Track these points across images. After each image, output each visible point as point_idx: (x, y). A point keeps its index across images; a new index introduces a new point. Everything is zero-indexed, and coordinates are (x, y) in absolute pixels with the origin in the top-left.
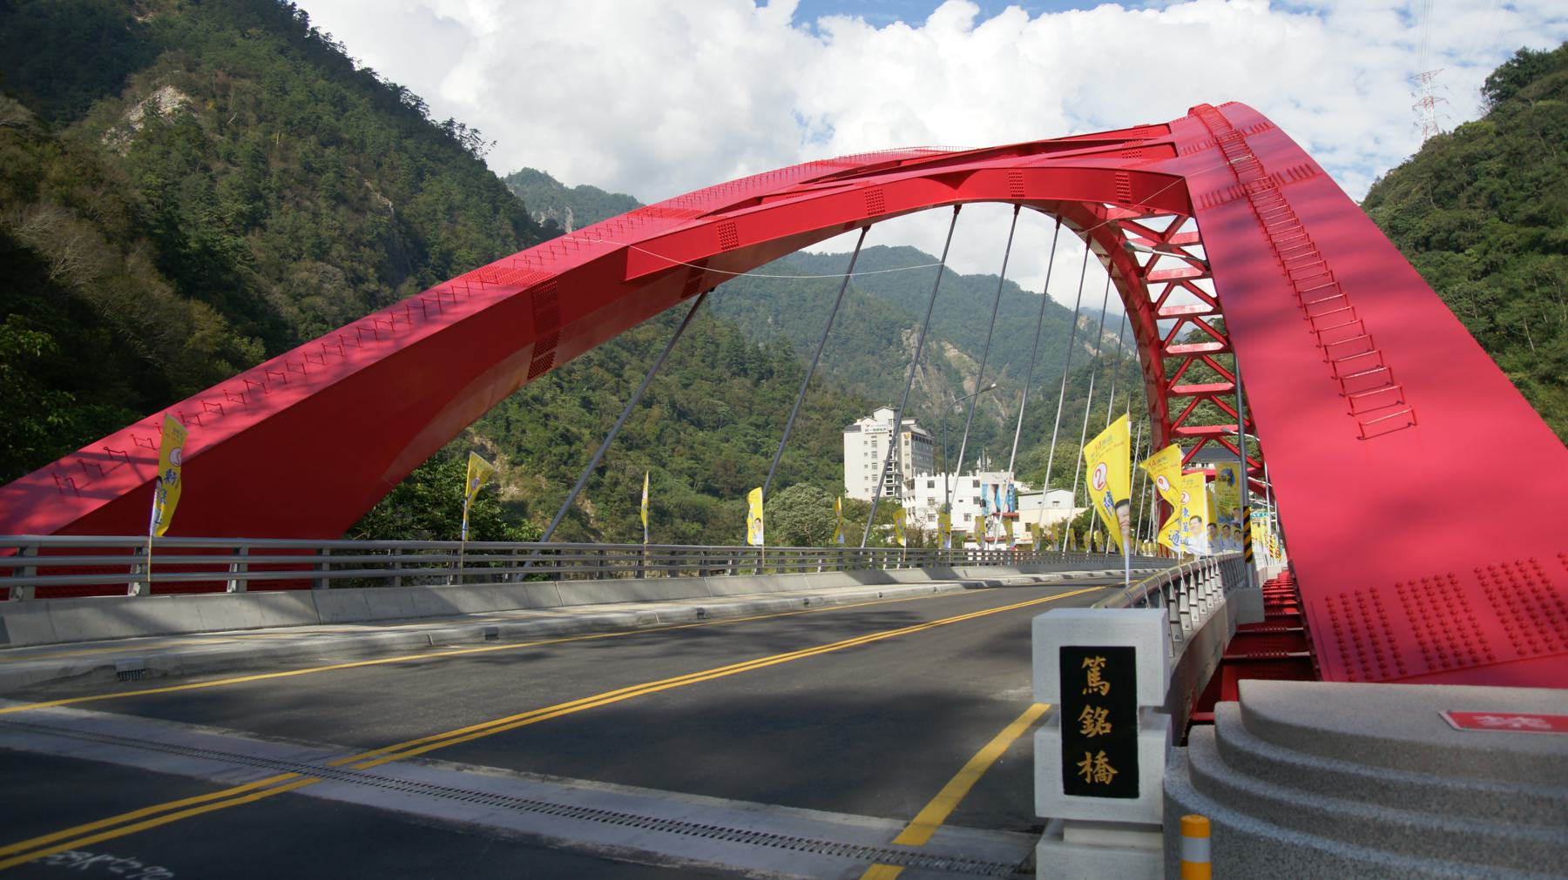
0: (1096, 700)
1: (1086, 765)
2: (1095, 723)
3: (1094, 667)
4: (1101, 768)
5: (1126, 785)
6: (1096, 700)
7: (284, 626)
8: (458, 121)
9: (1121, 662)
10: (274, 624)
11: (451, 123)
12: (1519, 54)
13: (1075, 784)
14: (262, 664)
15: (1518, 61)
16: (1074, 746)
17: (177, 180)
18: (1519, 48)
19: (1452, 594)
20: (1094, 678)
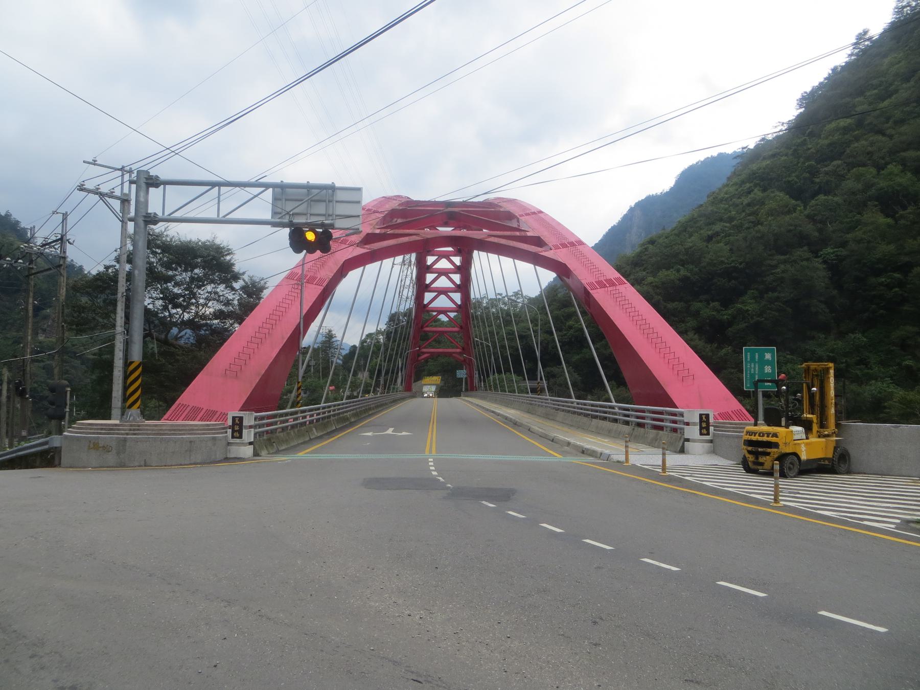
0: (704, 422)
4: (704, 431)
5: (708, 434)
9: (707, 416)
13: (701, 434)
20: (704, 418)
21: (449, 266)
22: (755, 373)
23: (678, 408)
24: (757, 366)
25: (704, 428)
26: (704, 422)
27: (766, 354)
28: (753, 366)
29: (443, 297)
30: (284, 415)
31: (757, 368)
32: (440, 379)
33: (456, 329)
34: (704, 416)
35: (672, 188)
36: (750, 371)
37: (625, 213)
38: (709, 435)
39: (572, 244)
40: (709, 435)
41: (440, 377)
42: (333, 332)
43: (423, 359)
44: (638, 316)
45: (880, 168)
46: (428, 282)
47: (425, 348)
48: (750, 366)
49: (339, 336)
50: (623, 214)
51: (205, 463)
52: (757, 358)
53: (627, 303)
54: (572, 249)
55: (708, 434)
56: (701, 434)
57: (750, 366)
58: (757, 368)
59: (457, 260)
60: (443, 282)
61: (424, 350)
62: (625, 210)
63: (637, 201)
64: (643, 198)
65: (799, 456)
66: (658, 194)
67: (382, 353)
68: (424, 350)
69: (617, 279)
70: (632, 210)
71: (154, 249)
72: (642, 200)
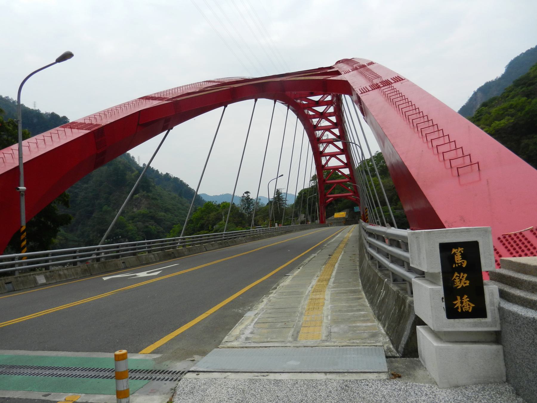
0: (460, 269)
20: (458, 259)
21: (333, 137)
23: (446, 228)
25: (463, 291)
26: (460, 269)
29: (333, 159)
30: (128, 246)
32: (345, 214)
35: (503, 74)
37: (471, 97)
38: (484, 315)
39: (387, 83)
40: (484, 315)
41: (345, 212)
42: (280, 191)
43: (329, 202)
44: (428, 121)
46: (321, 149)
49: (284, 191)
50: (469, 97)
51: (11, 292)
53: (401, 96)
54: (386, 89)
59: (336, 131)
60: (331, 149)
61: (329, 196)
62: (471, 94)
63: (478, 87)
66: (494, 80)
68: (329, 196)
70: (475, 94)
72: (482, 86)
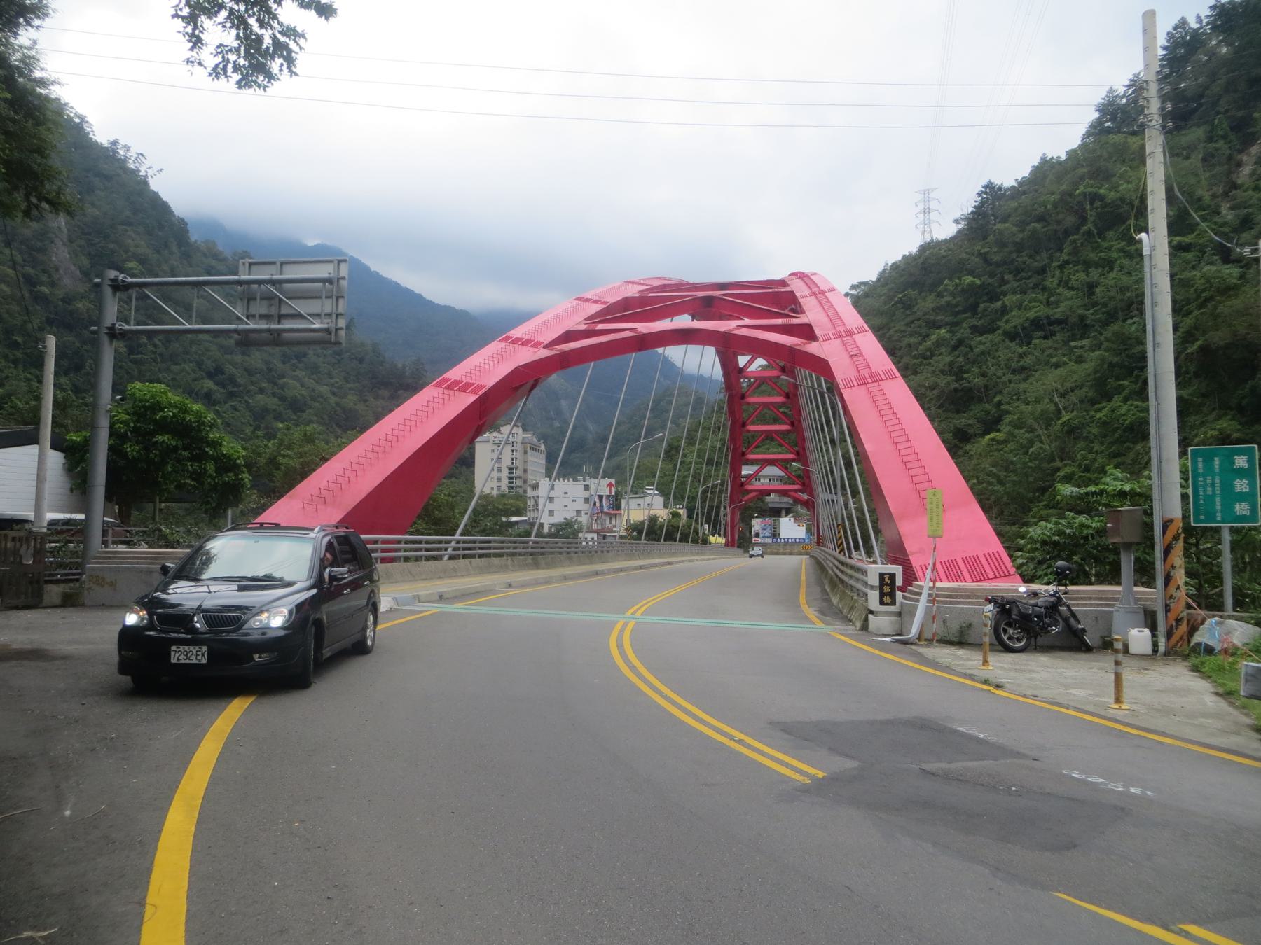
0: (887, 584)
1: (884, 599)
2: (887, 589)
3: (887, 577)
4: (887, 599)
5: (893, 603)
6: (887, 584)
7: (656, 565)
8: (122, 142)
9: (892, 576)
10: (1202, 740)
11: (115, 143)
12: (986, 187)
13: (882, 603)
14: (838, 421)
15: (986, 193)
16: (882, 595)
17: (351, 401)
18: (985, 182)
19: (994, 567)
20: (887, 580)
22: (1214, 494)
24: (1217, 481)
27: (1236, 457)
28: (1209, 480)
31: (1218, 486)
33: (780, 399)
34: (887, 577)
36: (1205, 491)
45: (974, 312)
47: (753, 423)
48: (1205, 481)
52: (1217, 467)
55: (893, 603)
56: (882, 603)
57: (1205, 481)
58: (1218, 486)
64: (1059, 151)
65: (995, 634)
67: (631, 470)
69: (886, 372)
71: (504, 519)
72: (1046, 170)
